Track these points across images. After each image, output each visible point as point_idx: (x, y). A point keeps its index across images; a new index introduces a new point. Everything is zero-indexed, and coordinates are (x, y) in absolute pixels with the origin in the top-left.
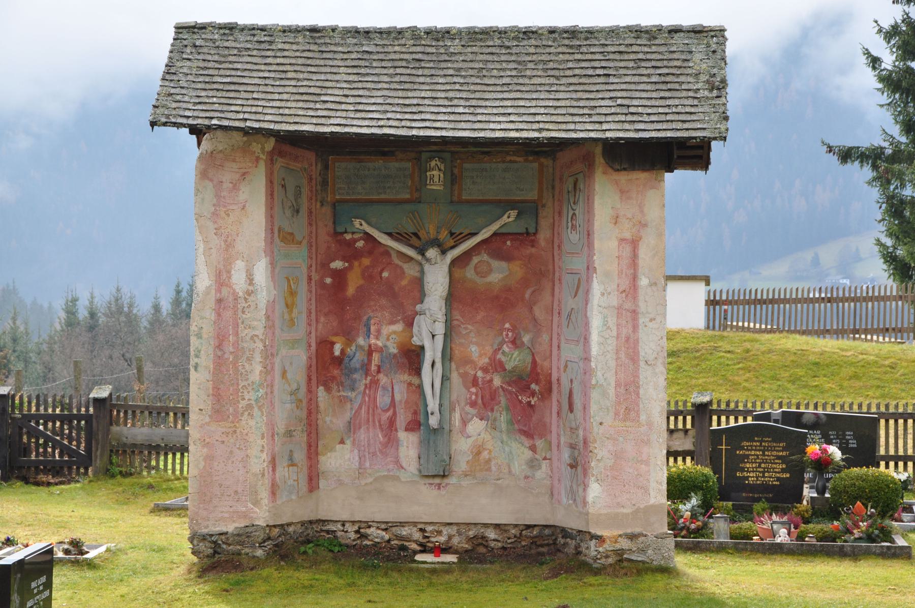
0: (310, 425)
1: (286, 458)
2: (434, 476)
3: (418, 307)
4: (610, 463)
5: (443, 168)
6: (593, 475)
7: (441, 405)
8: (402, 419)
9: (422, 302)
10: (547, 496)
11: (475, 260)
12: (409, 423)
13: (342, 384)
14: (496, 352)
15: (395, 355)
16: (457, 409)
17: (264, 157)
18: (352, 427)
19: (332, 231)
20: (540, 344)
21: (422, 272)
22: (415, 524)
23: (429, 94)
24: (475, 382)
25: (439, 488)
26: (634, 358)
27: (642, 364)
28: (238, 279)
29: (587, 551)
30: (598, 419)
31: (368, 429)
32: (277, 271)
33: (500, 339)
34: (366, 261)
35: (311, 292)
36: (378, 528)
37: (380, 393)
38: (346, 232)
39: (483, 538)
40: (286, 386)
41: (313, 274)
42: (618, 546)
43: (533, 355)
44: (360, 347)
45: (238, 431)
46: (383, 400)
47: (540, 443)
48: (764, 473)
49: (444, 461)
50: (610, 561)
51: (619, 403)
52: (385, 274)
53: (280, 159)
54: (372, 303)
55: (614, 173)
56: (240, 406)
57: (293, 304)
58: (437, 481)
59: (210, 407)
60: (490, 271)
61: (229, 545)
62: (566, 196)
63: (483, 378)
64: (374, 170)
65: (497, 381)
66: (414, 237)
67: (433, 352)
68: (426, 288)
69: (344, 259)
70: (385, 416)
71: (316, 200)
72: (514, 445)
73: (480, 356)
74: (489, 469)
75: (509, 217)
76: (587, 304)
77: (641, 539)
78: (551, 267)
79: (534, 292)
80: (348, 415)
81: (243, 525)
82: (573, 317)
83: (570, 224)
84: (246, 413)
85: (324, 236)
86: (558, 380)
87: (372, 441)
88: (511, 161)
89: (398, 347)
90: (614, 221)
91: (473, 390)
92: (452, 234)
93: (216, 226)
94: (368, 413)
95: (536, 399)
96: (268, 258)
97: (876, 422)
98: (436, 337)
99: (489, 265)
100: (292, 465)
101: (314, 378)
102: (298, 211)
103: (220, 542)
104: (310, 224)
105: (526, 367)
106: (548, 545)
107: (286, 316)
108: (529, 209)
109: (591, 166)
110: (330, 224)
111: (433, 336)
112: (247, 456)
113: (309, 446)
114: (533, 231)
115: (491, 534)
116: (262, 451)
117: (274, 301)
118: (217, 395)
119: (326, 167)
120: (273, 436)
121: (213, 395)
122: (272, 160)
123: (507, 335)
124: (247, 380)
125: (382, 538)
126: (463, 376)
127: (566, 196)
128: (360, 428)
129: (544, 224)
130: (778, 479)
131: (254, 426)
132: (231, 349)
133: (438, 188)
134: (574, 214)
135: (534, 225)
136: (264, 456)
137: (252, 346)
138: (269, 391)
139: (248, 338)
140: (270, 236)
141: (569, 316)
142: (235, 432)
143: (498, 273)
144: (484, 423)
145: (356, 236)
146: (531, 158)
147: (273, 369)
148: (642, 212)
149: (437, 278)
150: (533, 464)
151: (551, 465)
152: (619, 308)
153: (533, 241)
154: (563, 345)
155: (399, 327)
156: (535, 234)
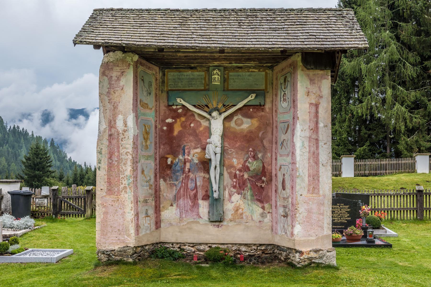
0: (156, 197)
1: (144, 213)
2: (216, 222)
3: (208, 140)
4: (305, 214)
5: (220, 74)
6: (297, 221)
7: (219, 187)
8: (201, 194)
9: (210, 138)
10: (270, 230)
11: (235, 118)
12: (204, 196)
13: (172, 177)
14: (245, 162)
15: (197, 164)
16: (227, 189)
17: (132, 64)
18: (176, 198)
19: (167, 105)
20: (267, 158)
21: (210, 124)
22: (206, 244)
23: (215, 31)
24: (235, 176)
25: (218, 227)
26: (317, 163)
27: (321, 165)
28: (120, 124)
29: (294, 258)
30: (300, 193)
31: (184, 199)
32: (139, 121)
33: (247, 156)
34: (183, 119)
35: (156, 133)
36: (189, 246)
37: (190, 182)
38: (173, 105)
39: (239, 250)
40: (144, 178)
41: (158, 124)
42: (310, 256)
43: (263, 163)
44: (179, 159)
45: (120, 200)
46: (191, 185)
47: (266, 205)
48: (341, 218)
49: (221, 214)
50: (306, 263)
51: (309, 185)
52: (192, 125)
53: (141, 67)
54: (186, 139)
55: (307, 71)
56: (121, 187)
57: (147, 138)
58: (217, 224)
59: (106, 188)
60: (242, 123)
61: (116, 256)
62: (279, 86)
63: (239, 174)
65: (246, 176)
66: (206, 107)
67: (215, 161)
68: (212, 131)
69: (173, 118)
70: (192, 193)
71: (159, 90)
72: (254, 206)
73: (238, 164)
74: (242, 218)
75: (251, 97)
76: (293, 136)
77: (321, 252)
79: (263, 133)
80: (174, 192)
81: (122, 246)
82: (285, 144)
83: (282, 99)
84: (124, 191)
85: (163, 108)
86: (276, 175)
87: (186, 205)
89: (198, 160)
90: (307, 94)
91: (235, 180)
92: (224, 105)
93: (109, 98)
94: (184, 191)
95: (264, 184)
96: (134, 114)
97: (369, 195)
98: (217, 155)
99: (242, 120)
100: (147, 217)
101: (158, 175)
102: (150, 94)
103: (111, 255)
104: (156, 101)
105: (260, 169)
106: (270, 253)
107: (144, 144)
108: (261, 93)
109: (294, 66)
110: (166, 101)
111: (216, 154)
112: (124, 212)
113: (156, 207)
115: (243, 249)
116: (131, 210)
117: (137, 135)
118: (109, 182)
119: (164, 75)
120: (137, 202)
121: (107, 182)
122: (137, 66)
123: (251, 154)
124: (124, 174)
125: (191, 251)
126: (230, 173)
127: (279, 86)
128: (180, 198)
129: (268, 100)
130: (346, 220)
131: (128, 197)
132: (116, 159)
133: (218, 83)
134: (285, 94)
135: (264, 101)
136: (132, 212)
137: (126, 157)
138: (135, 180)
139: (124, 153)
140: (135, 103)
141: (282, 143)
142: (118, 200)
143: (246, 125)
144: (240, 196)
145: (178, 107)
147: (137, 169)
148: (320, 90)
149: (217, 125)
150: (263, 215)
151: (272, 216)
152: (310, 137)
153: (263, 109)
154: (279, 158)
155: (199, 150)
156: (264, 105)
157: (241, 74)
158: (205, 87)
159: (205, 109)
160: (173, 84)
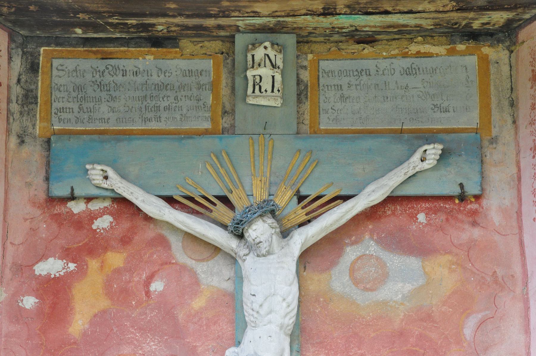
5: (280, 63)
11: (351, 253)
19: (42, 196)
21: (239, 279)
34: (116, 259)
38: (72, 198)
52: (157, 286)
60: (383, 277)
64: (136, 74)
69: (68, 254)
78: (517, 270)
79: (482, 323)
88: (419, 55)
92: (301, 198)
110: (39, 180)
114: (477, 192)
119: (33, 68)
129: (499, 177)
133: (272, 103)
135: (477, 178)
146: (461, 47)
153: (474, 213)
157: (369, 64)
158: (213, 120)
159: (214, 215)
160: (75, 106)
